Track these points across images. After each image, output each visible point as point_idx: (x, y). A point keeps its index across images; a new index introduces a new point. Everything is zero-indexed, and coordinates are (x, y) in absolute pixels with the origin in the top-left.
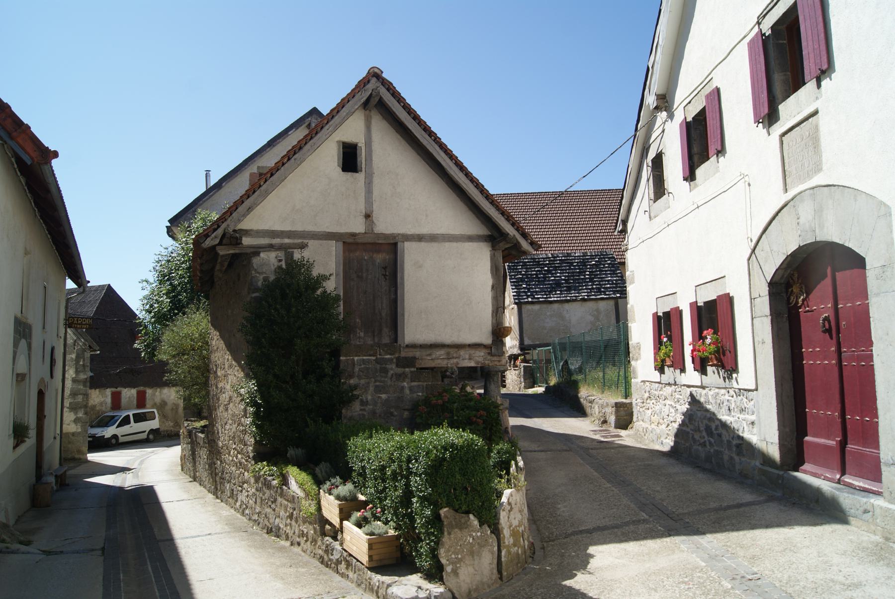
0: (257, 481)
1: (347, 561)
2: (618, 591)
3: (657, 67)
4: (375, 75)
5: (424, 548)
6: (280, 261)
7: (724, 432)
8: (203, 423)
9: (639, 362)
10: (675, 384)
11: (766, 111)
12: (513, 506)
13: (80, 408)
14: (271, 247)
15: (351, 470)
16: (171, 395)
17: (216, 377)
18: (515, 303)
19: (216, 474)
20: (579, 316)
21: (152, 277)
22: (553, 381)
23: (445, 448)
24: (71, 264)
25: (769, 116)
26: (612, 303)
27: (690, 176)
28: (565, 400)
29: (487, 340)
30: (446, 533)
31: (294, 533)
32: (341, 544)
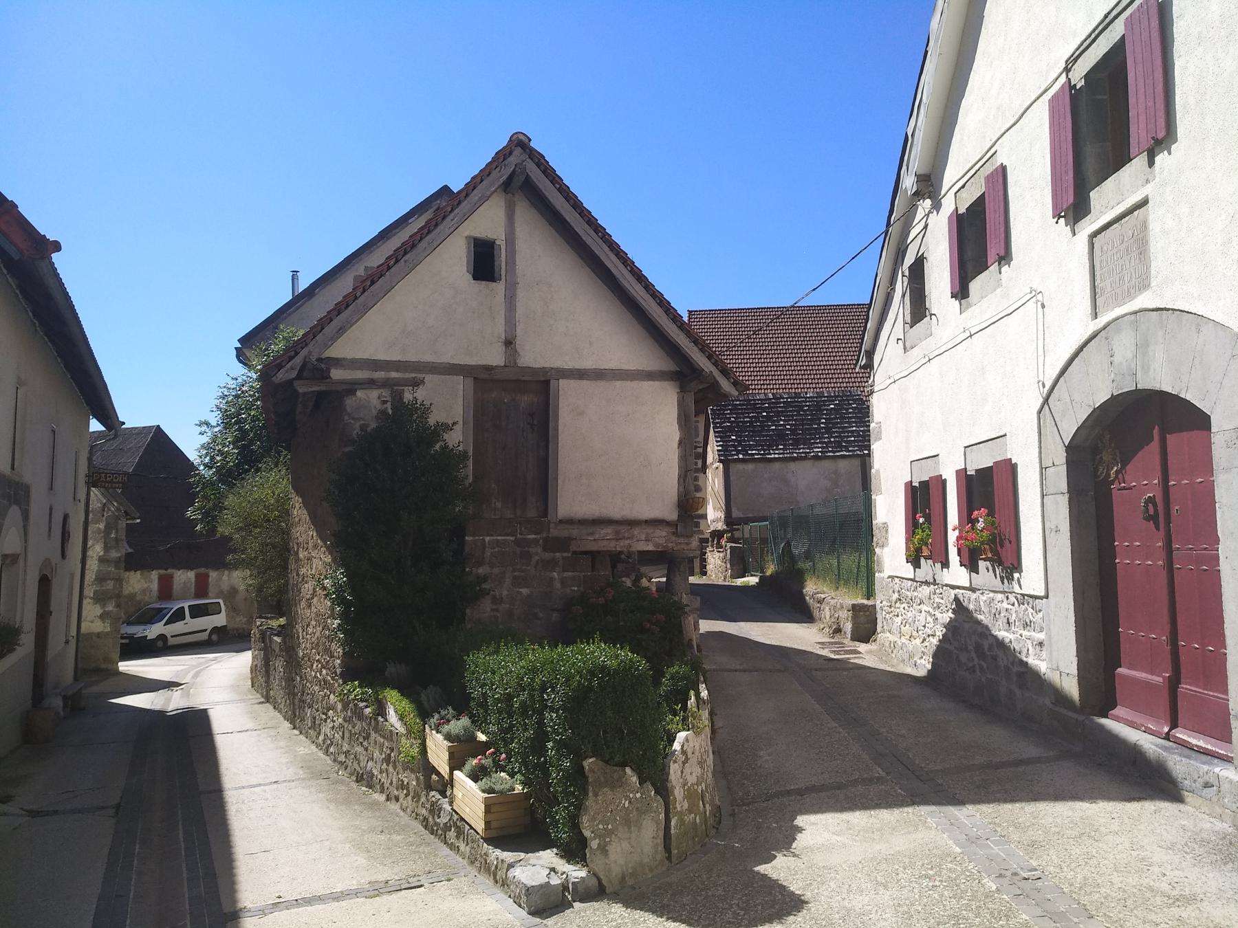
0: (345, 708)
1: (458, 827)
2: (832, 884)
3: (919, 136)
4: (520, 143)
5: (561, 814)
6: (385, 402)
7: (1000, 654)
8: (282, 621)
9: (885, 549)
10: (935, 583)
11: (1071, 200)
12: (690, 755)
13: (111, 598)
14: (371, 383)
15: (468, 698)
16: (239, 579)
17: (298, 560)
18: (720, 461)
19: (294, 695)
20: (808, 480)
21: (214, 418)
22: (770, 570)
23: (592, 673)
24: (96, 399)
25: (1073, 208)
26: (857, 462)
27: (961, 292)
28: (785, 600)
29: (673, 516)
30: (590, 794)
31: (391, 783)
32: (451, 803)
